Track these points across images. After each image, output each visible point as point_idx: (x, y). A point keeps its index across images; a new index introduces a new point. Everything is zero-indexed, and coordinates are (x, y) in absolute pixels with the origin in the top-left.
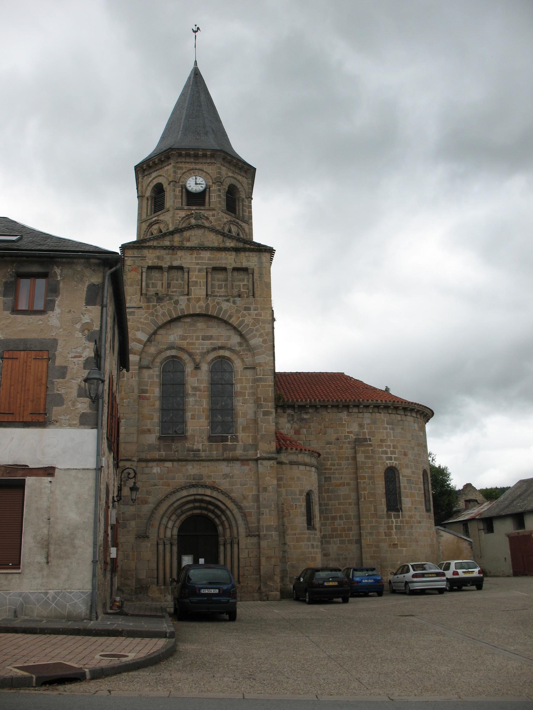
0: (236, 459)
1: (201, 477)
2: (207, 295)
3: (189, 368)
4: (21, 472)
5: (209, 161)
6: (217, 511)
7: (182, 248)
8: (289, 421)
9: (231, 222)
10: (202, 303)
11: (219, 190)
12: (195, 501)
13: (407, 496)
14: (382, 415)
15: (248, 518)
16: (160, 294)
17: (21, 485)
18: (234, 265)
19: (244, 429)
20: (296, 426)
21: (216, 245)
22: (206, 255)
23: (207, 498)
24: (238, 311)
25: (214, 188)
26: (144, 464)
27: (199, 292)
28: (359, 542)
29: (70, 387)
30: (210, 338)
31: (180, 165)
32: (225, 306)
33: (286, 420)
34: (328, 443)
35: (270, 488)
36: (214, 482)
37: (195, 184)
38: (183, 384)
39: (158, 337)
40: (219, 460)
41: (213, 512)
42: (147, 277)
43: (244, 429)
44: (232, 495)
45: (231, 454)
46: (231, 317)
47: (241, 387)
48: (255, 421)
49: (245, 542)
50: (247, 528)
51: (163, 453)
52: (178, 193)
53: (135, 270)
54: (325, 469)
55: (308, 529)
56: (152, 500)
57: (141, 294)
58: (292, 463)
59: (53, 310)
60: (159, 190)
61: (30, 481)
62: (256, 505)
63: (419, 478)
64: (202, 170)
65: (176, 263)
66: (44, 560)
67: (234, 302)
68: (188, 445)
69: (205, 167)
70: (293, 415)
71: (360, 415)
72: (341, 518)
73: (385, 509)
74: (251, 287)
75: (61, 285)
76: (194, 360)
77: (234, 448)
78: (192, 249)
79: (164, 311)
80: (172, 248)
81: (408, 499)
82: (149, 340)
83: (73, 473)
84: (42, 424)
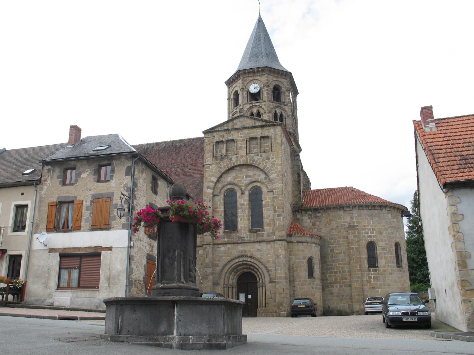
1: (245, 251)
2: (247, 153)
3: (239, 194)
4: (100, 249)
6: (255, 269)
8: (309, 218)
10: (244, 158)
11: (267, 90)
12: (243, 264)
13: (382, 259)
14: (365, 211)
15: (270, 273)
17: (99, 255)
19: (268, 225)
20: (313, 221)
21: (251, 125)
22: (246, 131)
23: (249, 263)
24: (263, 160)
25: (265, 89)
26: (216, 246)
27: (242, 152)
28: (350, 286)
29: (86, 214)
30: (249, 176)
31: (246, 79)
32: (256, 158)
33: (307, 218)
35: (281, 256)
36: (252, 254)
37: (254, 88)
38: (236, 203)
39: (223, 179)
40: (254, 242)
41: (254, 270)
43: (268, 225)
45: (261, 239)
46: (259, 164)
47: (266, 202)
48: (274, 219)
49: (268, 285)
52: (245, 95)
53: (210, 144)
54: (331, 244)
55: (309, 278)
56: (221, 265)
58: (298, 242)
60: (236, 94)
61: (103, 253)
63: (392, 247)
65: (230, 138)
66: (108, 285)
67: (261, 156)
68: (239, 235)
70: (311, 215)
71: (351, 212)
72: (340, 272)
73: (367, 267)
75: (116, 168)
77: (263, 236)
78: (238, 129)
79: (225, 164)
80: (228, 130)
81: (382, 260)
82: (218, 181)
83: (119, 249)
84: (108, 229)
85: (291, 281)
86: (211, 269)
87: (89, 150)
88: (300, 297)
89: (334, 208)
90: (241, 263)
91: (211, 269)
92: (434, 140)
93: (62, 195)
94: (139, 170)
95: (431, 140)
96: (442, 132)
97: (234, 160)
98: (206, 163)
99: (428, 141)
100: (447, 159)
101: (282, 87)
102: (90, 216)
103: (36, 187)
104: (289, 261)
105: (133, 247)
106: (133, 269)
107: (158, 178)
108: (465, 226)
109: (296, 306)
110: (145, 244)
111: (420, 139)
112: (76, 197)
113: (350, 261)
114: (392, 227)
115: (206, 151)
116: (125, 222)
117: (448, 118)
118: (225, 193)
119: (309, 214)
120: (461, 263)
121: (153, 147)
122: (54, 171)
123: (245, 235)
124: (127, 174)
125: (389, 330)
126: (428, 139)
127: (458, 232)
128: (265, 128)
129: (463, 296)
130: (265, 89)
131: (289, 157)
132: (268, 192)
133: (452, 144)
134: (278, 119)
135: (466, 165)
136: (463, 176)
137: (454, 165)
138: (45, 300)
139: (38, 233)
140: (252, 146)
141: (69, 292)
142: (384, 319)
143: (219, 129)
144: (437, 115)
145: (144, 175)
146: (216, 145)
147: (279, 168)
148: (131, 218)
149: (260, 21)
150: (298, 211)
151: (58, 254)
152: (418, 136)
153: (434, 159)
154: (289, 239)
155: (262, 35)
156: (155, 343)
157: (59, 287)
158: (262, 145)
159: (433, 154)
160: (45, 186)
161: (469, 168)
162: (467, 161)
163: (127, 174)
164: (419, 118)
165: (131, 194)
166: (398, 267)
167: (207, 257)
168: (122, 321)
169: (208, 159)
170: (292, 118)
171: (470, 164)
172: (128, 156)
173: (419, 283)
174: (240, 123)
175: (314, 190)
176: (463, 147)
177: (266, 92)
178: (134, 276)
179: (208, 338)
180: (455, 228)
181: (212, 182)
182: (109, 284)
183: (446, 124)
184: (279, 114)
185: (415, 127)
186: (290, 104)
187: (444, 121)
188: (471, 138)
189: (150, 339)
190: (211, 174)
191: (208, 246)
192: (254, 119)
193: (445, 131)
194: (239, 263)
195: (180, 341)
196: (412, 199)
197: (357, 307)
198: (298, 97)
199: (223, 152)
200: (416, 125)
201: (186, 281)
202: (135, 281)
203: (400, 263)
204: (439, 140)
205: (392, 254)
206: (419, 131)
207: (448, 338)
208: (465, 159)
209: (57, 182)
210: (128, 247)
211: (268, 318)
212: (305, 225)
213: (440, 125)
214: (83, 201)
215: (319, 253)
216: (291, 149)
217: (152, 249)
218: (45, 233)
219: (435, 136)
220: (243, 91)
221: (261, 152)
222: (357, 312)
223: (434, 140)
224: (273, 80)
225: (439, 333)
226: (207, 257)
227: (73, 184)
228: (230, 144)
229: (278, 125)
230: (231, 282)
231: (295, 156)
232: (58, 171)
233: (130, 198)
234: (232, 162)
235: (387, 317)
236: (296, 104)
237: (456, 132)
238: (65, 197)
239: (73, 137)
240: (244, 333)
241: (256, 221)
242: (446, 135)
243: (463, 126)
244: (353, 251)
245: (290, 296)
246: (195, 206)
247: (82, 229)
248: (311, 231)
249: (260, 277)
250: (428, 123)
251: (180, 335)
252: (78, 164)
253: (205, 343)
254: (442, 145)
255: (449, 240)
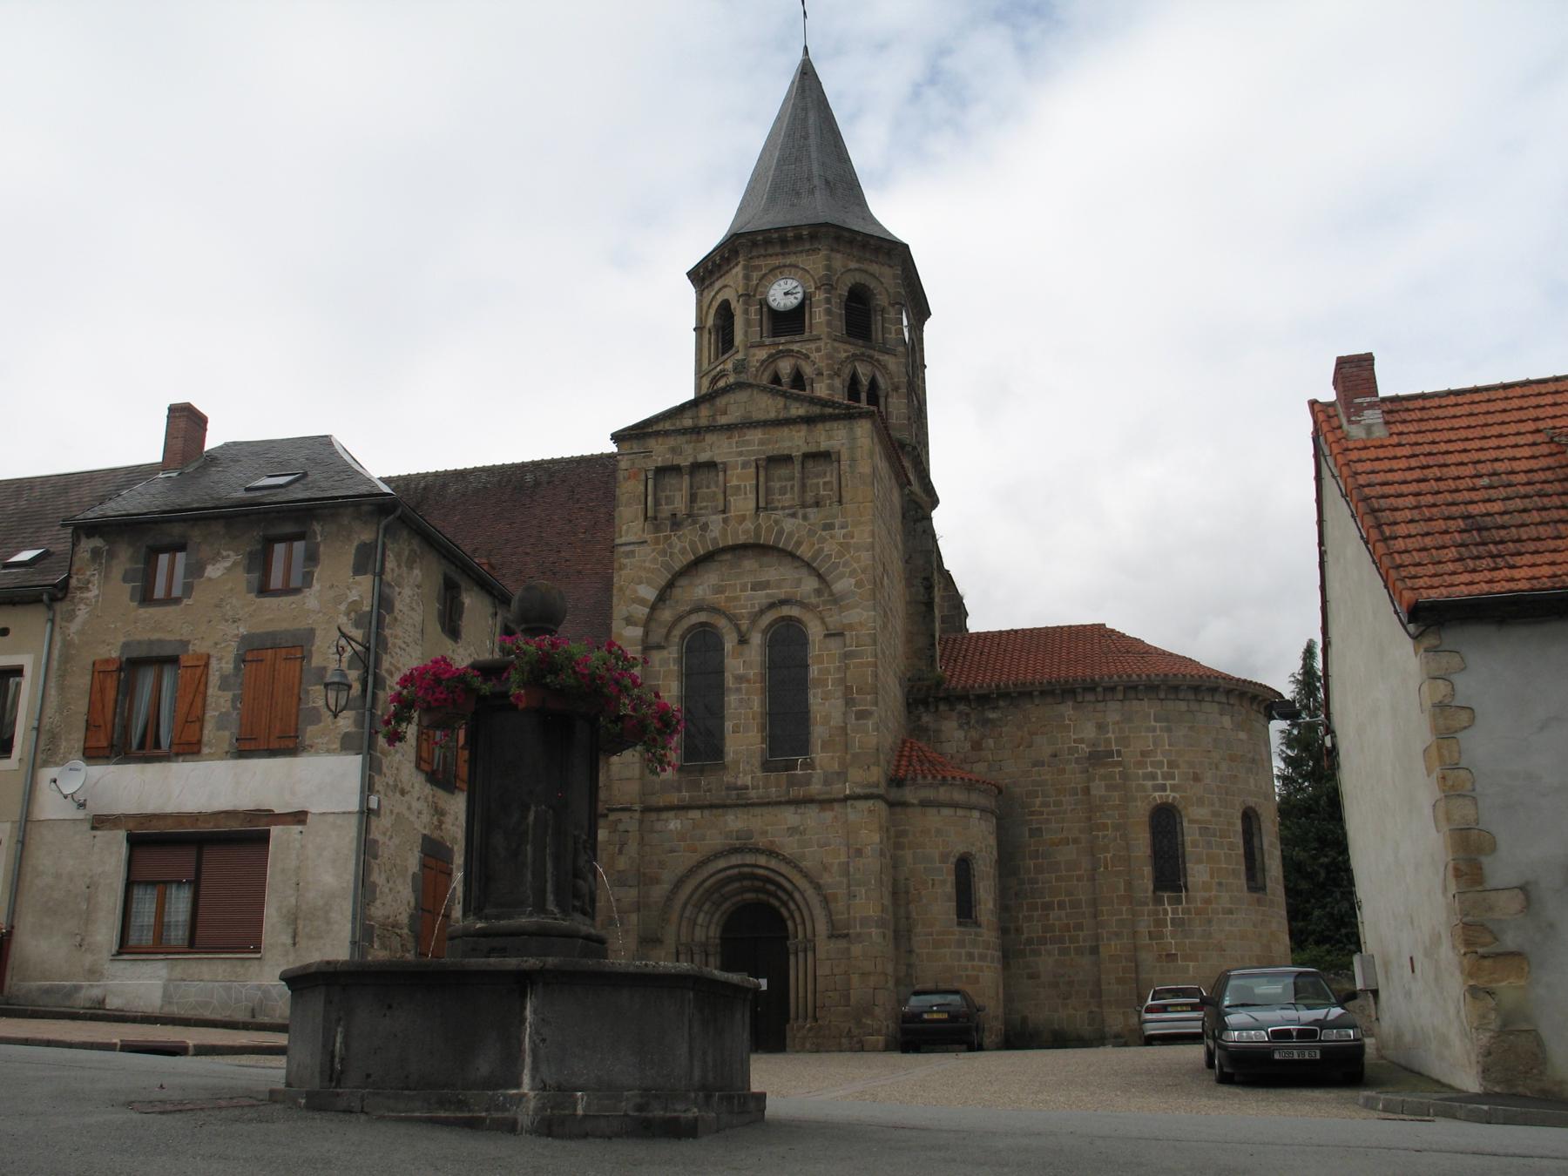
0: (809, 801)
1: (749, 834)
2: (758, 508)
3: (729, 646)
5: (807, 247)
6: (780, 893)
7: (712, 429)
8: (961, 727)
9: (855, 357)
10: (749, 525)
11: (828, 301)
13: (1199, 861)
14: (1146, 703)
15: (832, 906)
16: (679, 516)
17: (263, 839)
18: (805, 449)
19: (825, 746)
20: (974, 734)
21: (773, 415)
22: (756, 436)
23: (761, 871)
24: (812, 533)
26: (653, 816)
27: (743, 504)
28: (1095, 950)
29: (219, 701)
31: (757, 262)
32: (789, 525)
33: (955, 724)
34: (1038, 763)
35: (868, 850)
36: (772, 842)
37: (782, 294)
38: (720, 671)
39: (677, 592)
40: (779, 803)
42: (655, 486)
43: (825, 746)
44: (803, 864)
46: (799, 544)
47: (820, 671)
48: (844, 729)
49: (824, 947)
50: (831, 923)
51: (686, 795)
52: (754, 317)
54: (1032, 813)
55: (959, 924)
56: (668, 877)
57: (646, 518)
58: (925, 804)
59: (310, 586)
60: (725, 312)
61: (275, 831)
62: (845, 880)
64: (796, 266)
65: (703, 457)
66: (289, 941)
67: (805, 517)
68: (728, 778)
69: (801, 260)
70: (968, 715)
71: (1100, 706)
72: (1061, 905)
73: (1151, 887)
74: (835, 486)
75: (322, 549)
76: (737, 627)
77: (807, 781)
78: (729, 428)
79: (684, 545)
80: (696, 431)
81: (1201, 867)
82: (662, 597)
83: (331, 819)
85: (901, 933)
86: (633, 892)
87: (231, 487)
88: (930, 986)
89: (1042, 693)
90: (736, 871)
91: (633, 892)
92: (1377, 466)
93: (138, 637)
94: (398, 556)
95: (1368, 466)
96: (1404, 440)
97: (715, 531)
98: (623, 540)
99: (1360, 467)
100: (1422, 527)
101: (877, 295)
102: (235, 708)
103: (50, 607)
104: (895, 867)
105: (377, 813)
106: (374, 885)
107: (463, 585)
108: (1478, 746)
109: (916, 1017)
110: (416, 805)
111: (1331, 464)
112: (185, 644)
113: (1094, 869)
114: (1232, 759)
115: (624, 499)
116: (352, 729)
117: (1423, 396)
118: (683, 637)
119: (960, 713)
120: (1463, 867)
121: (444, 486)
122: (112, 555)
123: (748, 780)
124: (359, 569)
125: (1225, 1089)
126: (1360, 461)
127: (1456, 767)
128: (820, 426)
129: (1471, 975)
130: (820, 296)
131: (896, 523)
132: (827, 636)
133: (1438, 479)
134: (863, 396)
135: (1481, 548)
136: (1472, 583)
137: (1444, 547)
138: (77, 988)
139: (57, 764)
140: (776, 485)
141: (160, 964)
142: (1210, 1055)
143: (667, 426)
144: (1388, 386)
145: (417, 572)
146: (655, 479)
147: (865, 557)
148: (372, 715)
149: (807, 80)
150: (925, 703)
151: (122, 835)
152: (1327, 452)
153: (1379, 526)
154: (895, 794)
155: (812, 118)
156: (459, 1115)
157: (125, 947)
158: (809, 482)
159: (1374, 511)
160: (82, 606)
161: (1493, 556)
162: (1485, 534)
163: (359, 569)
164: (1328, 395)
165: (373, 636)
166: (1251, 889)
167: (620, 852)
168: (346, 1043)
169: (630, 526)
170: (909, 395)
171: (1496, 543)
172: (365, 508)
173: (1318, 943)
174: (735, 408)
175: (978, 634)
176: (1474, 489)
177: (818, 308)
178: (378, 911)
179: (638, 1100)
180: (1446, 753)
181: (642, 602)
182: (294, 937)
183: (1418, 415)
184: (865, 381)
185: (1315, 422)
186: (901, 349)
187: (1411, 405)
188: (1497, 460)
189: (442, 1104)
190: (637, 580)
191: (625, 816)
192: (784, 395)
193: (1413, 438)
194: (729, 872)
195: (543, 1108)
196: (1297, 666)
197: (1116, 1021)
198: (929, 327)
199: (680, 504)
200: (1321, 417)
201: (564, 911)
202: (383, 926)
203: (1259, 875)
204: (1395, 465)
205: (1232, 846)
206: (1330, 437)
207: (1420, 1113)
208: (1479, 530)
209: (122, 592)
210: (361, 812)
211: (824, 1056)
212: (949, 748)
213: (1397, 417)
214: (209, 656)
215: (992, 841)
216: (902, 496)
217: (441, 823)
218: (81, 764)
219: (1381, 453)
220: (746, 303)
221: (804, 506)
222: (1117, 1036)
223: (1377, 466)
224: (849, 269)
225: (1389, 1096)
226: (620, 852)
227: (177, 601)
228: (702, 477)
229: (862, 415)
230: (700, 934)
231: (915, 521)
232: (125, 558)
233: (368, 649)
234: (710, 535)
235: (1220, 1047)
236: (922, 350)
237: (1450, 441)
238: (151, 643)
239: (179, 443)
240: (755, 1087)
241: (787, 731)
242: (1418, 450)
243: (1472, 421)
244: (1105, 837)
245: (898, 982)
246: (596, 656)
247: (205, 750)
248: (967, 767)
249: (798, 920)
250: (1360, 409)
251: (544, 1089)
252: (196, 534)
253: (626, 1115)
254: (1405, 482)
255: (1426, 792)
